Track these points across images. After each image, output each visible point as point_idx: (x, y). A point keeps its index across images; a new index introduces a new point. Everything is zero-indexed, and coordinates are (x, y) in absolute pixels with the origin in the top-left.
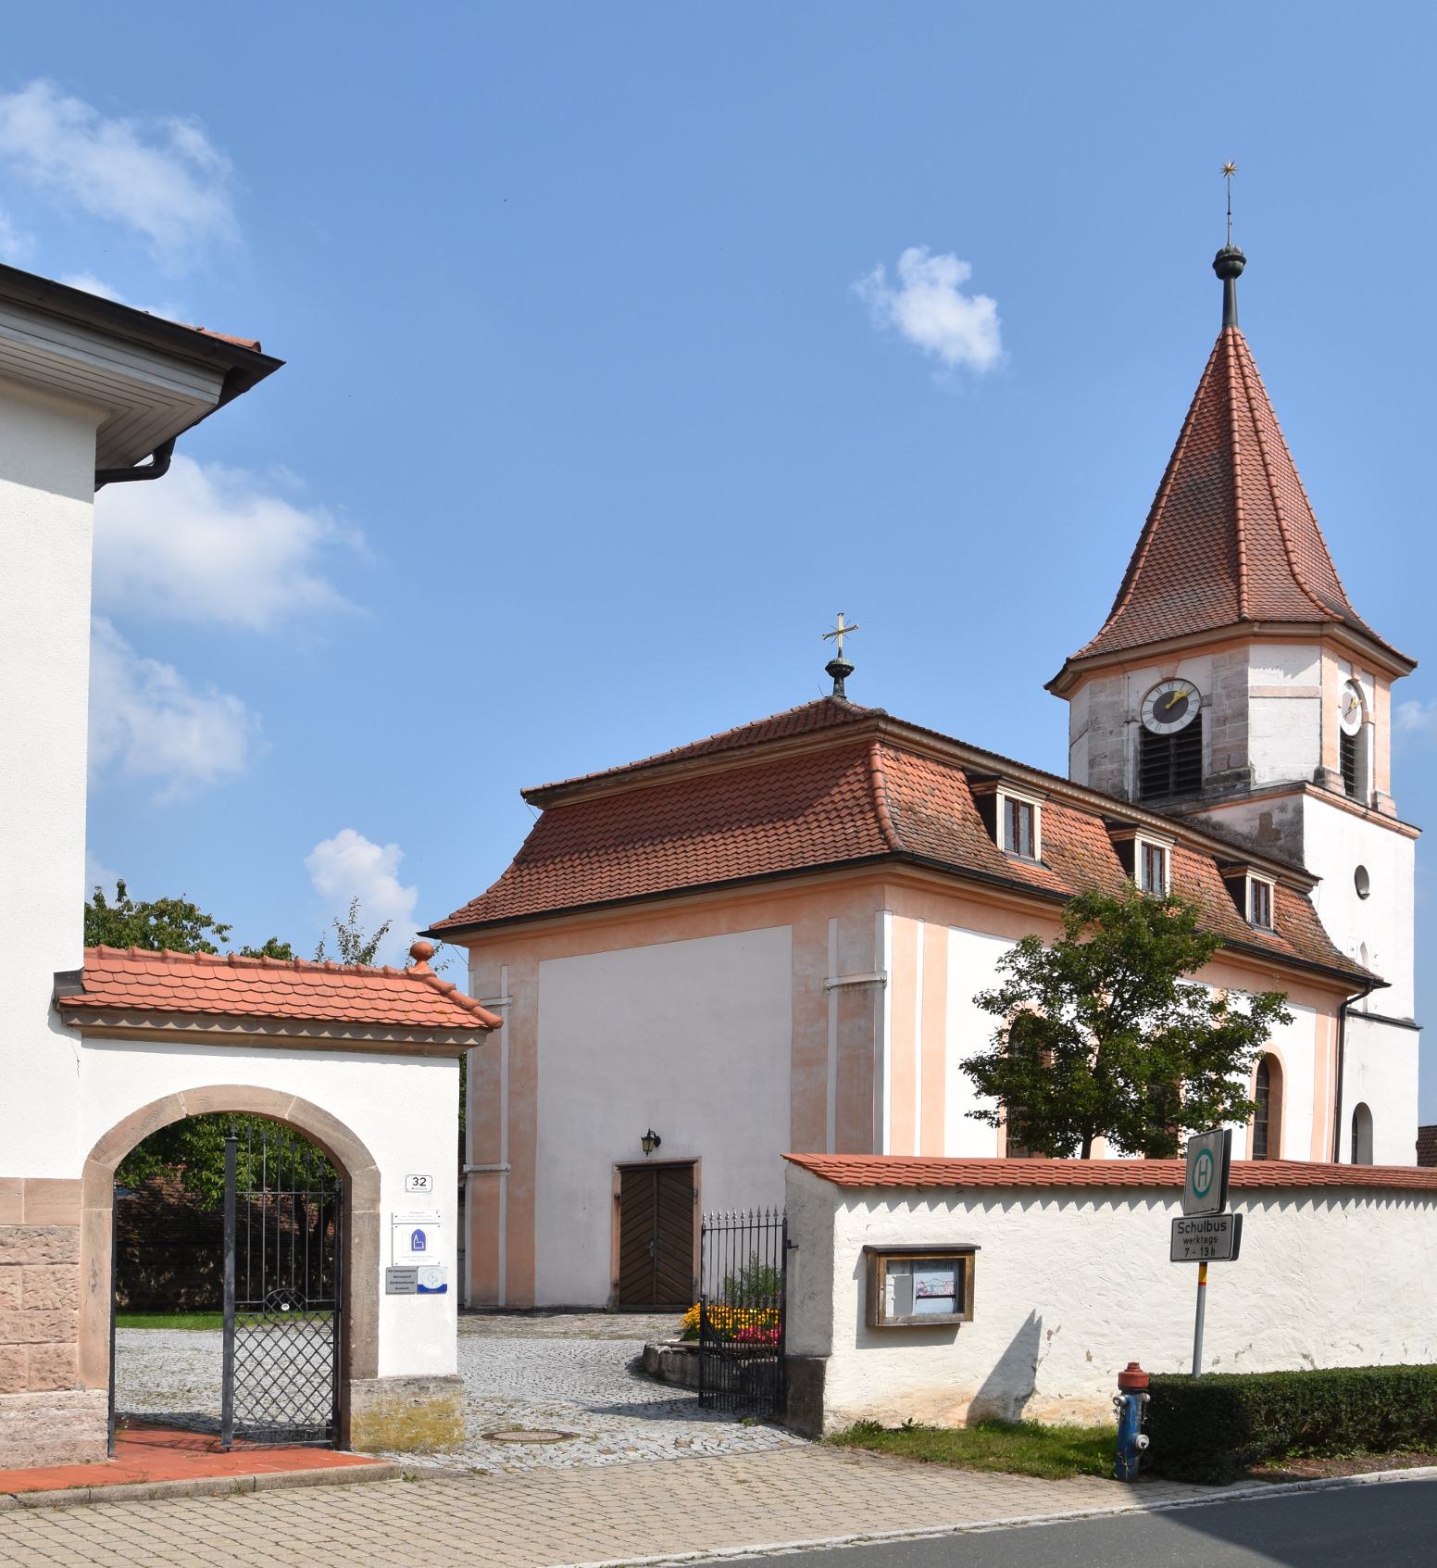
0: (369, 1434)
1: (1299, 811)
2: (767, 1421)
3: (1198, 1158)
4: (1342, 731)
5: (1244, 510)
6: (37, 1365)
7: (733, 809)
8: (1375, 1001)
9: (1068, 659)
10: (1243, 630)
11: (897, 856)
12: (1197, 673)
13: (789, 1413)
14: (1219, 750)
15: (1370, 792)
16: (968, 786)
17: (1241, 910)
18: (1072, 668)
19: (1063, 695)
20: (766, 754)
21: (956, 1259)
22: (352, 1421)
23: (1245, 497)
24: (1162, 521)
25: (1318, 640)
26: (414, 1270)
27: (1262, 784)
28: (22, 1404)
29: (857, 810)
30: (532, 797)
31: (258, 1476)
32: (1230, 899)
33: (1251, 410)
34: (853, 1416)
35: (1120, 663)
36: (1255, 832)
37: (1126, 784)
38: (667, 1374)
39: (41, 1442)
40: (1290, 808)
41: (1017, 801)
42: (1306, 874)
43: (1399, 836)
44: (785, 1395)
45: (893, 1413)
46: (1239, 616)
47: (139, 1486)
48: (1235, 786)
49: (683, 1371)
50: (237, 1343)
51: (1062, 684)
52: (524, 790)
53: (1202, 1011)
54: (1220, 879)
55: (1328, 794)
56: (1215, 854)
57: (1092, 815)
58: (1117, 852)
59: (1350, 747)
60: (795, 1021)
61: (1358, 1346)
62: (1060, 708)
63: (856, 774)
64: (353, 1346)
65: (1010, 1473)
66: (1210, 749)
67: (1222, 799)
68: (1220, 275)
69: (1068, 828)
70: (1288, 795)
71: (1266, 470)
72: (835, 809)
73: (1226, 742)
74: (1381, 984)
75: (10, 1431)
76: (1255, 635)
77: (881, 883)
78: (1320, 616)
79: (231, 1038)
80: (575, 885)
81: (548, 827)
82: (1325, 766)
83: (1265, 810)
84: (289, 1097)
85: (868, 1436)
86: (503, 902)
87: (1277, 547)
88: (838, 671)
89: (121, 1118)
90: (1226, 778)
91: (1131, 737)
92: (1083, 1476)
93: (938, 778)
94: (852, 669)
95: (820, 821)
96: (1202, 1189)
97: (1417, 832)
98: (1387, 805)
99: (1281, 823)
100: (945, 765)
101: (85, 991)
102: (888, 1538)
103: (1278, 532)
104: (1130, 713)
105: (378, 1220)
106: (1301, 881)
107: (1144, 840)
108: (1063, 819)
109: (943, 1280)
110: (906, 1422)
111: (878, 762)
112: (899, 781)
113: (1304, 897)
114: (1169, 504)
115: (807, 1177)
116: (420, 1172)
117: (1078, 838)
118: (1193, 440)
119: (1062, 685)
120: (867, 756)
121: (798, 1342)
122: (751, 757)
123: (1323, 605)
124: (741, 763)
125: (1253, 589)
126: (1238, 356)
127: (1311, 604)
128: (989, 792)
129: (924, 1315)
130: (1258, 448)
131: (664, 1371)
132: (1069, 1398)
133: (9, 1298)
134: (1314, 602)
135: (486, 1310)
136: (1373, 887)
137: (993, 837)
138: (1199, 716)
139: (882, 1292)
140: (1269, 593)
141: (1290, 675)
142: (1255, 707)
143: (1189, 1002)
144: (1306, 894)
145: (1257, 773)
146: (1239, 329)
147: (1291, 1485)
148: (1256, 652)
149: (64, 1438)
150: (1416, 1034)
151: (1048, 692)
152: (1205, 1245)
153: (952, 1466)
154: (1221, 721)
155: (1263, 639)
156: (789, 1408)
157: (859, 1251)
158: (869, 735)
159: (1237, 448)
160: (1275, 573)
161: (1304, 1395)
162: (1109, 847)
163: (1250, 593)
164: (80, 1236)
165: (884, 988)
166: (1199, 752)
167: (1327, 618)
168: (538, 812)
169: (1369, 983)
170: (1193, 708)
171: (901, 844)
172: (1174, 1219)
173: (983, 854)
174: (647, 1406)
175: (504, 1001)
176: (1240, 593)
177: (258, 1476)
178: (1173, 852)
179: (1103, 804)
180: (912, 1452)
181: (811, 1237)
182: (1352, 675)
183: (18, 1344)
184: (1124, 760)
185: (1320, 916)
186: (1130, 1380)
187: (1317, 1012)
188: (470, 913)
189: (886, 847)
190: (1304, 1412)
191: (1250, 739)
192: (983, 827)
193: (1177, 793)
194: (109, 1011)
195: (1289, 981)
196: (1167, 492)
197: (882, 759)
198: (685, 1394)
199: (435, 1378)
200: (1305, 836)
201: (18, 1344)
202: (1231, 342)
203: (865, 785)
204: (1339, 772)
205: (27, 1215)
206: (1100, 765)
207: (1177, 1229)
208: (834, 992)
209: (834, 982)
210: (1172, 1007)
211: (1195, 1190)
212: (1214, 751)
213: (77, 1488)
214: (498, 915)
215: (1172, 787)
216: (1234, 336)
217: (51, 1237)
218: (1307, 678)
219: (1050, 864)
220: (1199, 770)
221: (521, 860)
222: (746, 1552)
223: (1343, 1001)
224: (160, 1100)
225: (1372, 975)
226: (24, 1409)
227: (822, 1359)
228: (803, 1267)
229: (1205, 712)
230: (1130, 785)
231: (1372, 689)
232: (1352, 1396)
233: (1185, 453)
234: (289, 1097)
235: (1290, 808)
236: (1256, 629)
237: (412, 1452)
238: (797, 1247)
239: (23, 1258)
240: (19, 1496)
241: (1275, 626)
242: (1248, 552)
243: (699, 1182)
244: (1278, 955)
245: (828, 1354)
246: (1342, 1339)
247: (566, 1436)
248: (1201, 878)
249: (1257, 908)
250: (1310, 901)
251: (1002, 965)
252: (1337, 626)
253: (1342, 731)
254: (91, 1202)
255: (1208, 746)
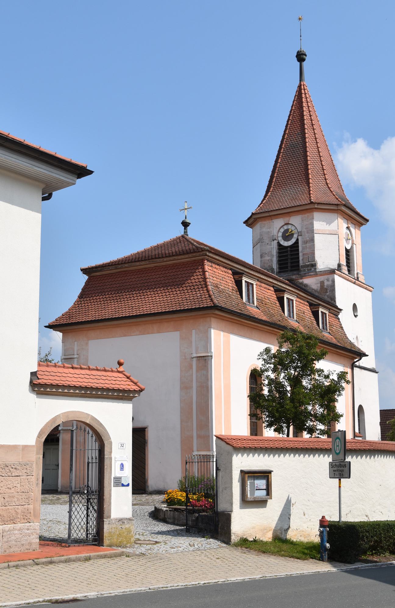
0: (109, 540)
1: (333, 281)
2: (212, 537)
3: (336, 440)
4: (345, 247)
5: (309, 156)
6: (23, 514)
7: (157, 282)
8: (363, 362)
9: (252, 213)
10: (311, 206)
11: (215, 307)
12: (296, 221)
13: (219, 534)
14: (305, 254)
15: (356, 272)
16: (233, 276)
17: (318, 324)
18: (254, 217)
19: (250, 226)
20: (168, 261)
21: (266, 475)
22: (104, 535)
23: (310, 151)
24: (282, 158)
25: (336, 211)
26: (120, 478)
27: (320, 269)
28: (19, 528)
29: (200, 286)
30: (85, 271)
31: (91, 554)
32: (314, 319)
33: (310, 116)
34: (240, 536)
35: (270, 216)
36: (319, 289)
37: (273, 265)
38: (167, 519)
39: (23, 543)
40: (330, 279)
41: (248, 282)
42: (336, 307)
43: (366, 290)
44: (218, 527)
45: (250, 535)
46: (310, 200)
47: (63, 557)
48: (311, 269)
49: (174, 518)
50: (73, 505)
51: (250, 222)
52: (82, 268)
53: (322, 378)
54: (310, 311)
55: (342, 274)
56: (308, 300)
57: (270, 286)
58: (279, 301)
59: (348, 253)
60: (181, 371)
62: (249, 231)
63: (199, 272)
64: (105, 506)
65: (290, 557)
66: (302, 253)
67: (307, 274)
68: (298, 60)
69: (263, 292)
70: (329, 274)
71: (316, 141)
72: (193, 285)
73: (307, 251)
74: (365, 355)
75: (15, 538)
76: (316, 208)
77: (210, 317)
78: (336, 202)
79: (74, 394)
80: (102, 310)
81: (90, 283)
82: (341, 262)
83: (322, 280)
84: (88, 415)
85: (244, 543)
86: (76, 315)
87: (321, 172)
88: (185, 224)
89: (45, 423)
90: (308, 266)
91: (275, 246)
92: (311, 559)
93: (224, 273)
94: (190, 224)
95: (188, 290)
96: (338, 452)
97: (372, 289)
98: (361, 278)
99: (327, 286)
100: (226, 268)
101: (39, 379)
102: (270, 577)
103: (321, 166)
104: (274, 237)
105: (111, 459)
106: (336, 311)
107: (287, 297)
108: (261, 288)
109: (261, 483)
110: (254, 538)
111: (207, 268)
112: (213, 275)
113: (337, 317)
114: (284, 152)
115: (223, 443)
116: (122, 442)
117: (266, 296)
118: (291, 126)
119: (250, 222)
120: (203, 265)
121: (222, 506)
122: (163, 262)
123: (338, 197)
124: (159, 264)
125: (314, 189)
126: (305, 94)
127: (333, 196)
128: (240, 279)
129: (259, 497)
130: (313, 131)
131: (166, 518)
132: (299, 530)
133: (17, 488)
134: (334, 195)
135: (67, 492)
136: (359, 313)
137: (242, 297)
138: (297, 240)
139: (247, 487)
140: (319, 191)
142: (317, 237)
143: (318, 374)
144: (337, 316)
145: (318, 264)
146: (305, 82)
147: (371, 564)
148: (316, 215)
149: (29, 541)
151: (245, 225)
152: (340, 472)
153: (273, 555)
154: (305, 242)
155: (319, 210)
156: (219, 532)
157: (239, 472)
158: (203, 257)
159: (306, 131)
160: (321, 183)
161: (371, 530)
162: (276, 299)
163: (313, 191)
164: (34, 466)
165: (212, 359)
166: (298, 254)
167: (339, 203)
168: (86, 277)
169: (361, 355)
170: (295, 236)
171: (217, 302)
172: (330, 462)
173: (239, 304)
174: (173, 531)
175: (75, 356)
176: (310, 191)
177: (91, 554)
178: (296, 301)
179: (273, 282)
180: (260, 549)
181: (224, 466)
182: (348, 225)
183: (18, 506)
184: (273, 256)
185: (343, 325)
186: (323, 523)
188: (63, 319)
189: (212, 303)
190: (372, 537)
191: (315, 250)
192: (238, 293)
193: (291, 271)
194: (45, 386)
195: (335, 353)
196: (283, 147)
197: (208, 266)
198: (178, 528)
199: (126, 519)
200: (336, 291)
201: (18, 506)
202: (303, 88)
203: (202, 277)
204: (345, 265)
205: (22, 458)
206: (264, 257)
207: (331, 466)
208: (195, 359)
209: (195, 355)
210: (313, 376)
211: (336, 452)
212: (303, 254)
213: (47, 558)
214: (74, 321)
215: (289, 268)
216: (303, 85)
217: (27, 466)
218: (333, 226)
219: (259, 307)
220: (298, 262)
221: (81, 296)
222: (237, 580)
223: (353, 362)
224: (56, 416)
225: (362, 351)
226: (19, 530)
227: (230, 513)
228: (222, 477)
229: (300, 238)
230: (275, 266)
231: (354, 230)
232: (384, 531)
233: (289, 131)
234: (89, 415)
235: (330, 279)
236: (316, 206)
237: (120, 547)
238: (220, 470)
239: (21, 474)
240: (35, 560)
241: (322, 205)
242: (312, 174)
243: (147, 437)
244: (330, 343)
245: (232, 511)
246: (377, 509)
247: (157, 542)
248: (304, 311)
249: (323, 323)
250: (339, 319)
251: (259, 357)
253: (345, 247)
254: (37, 454)
255: (301, 252)
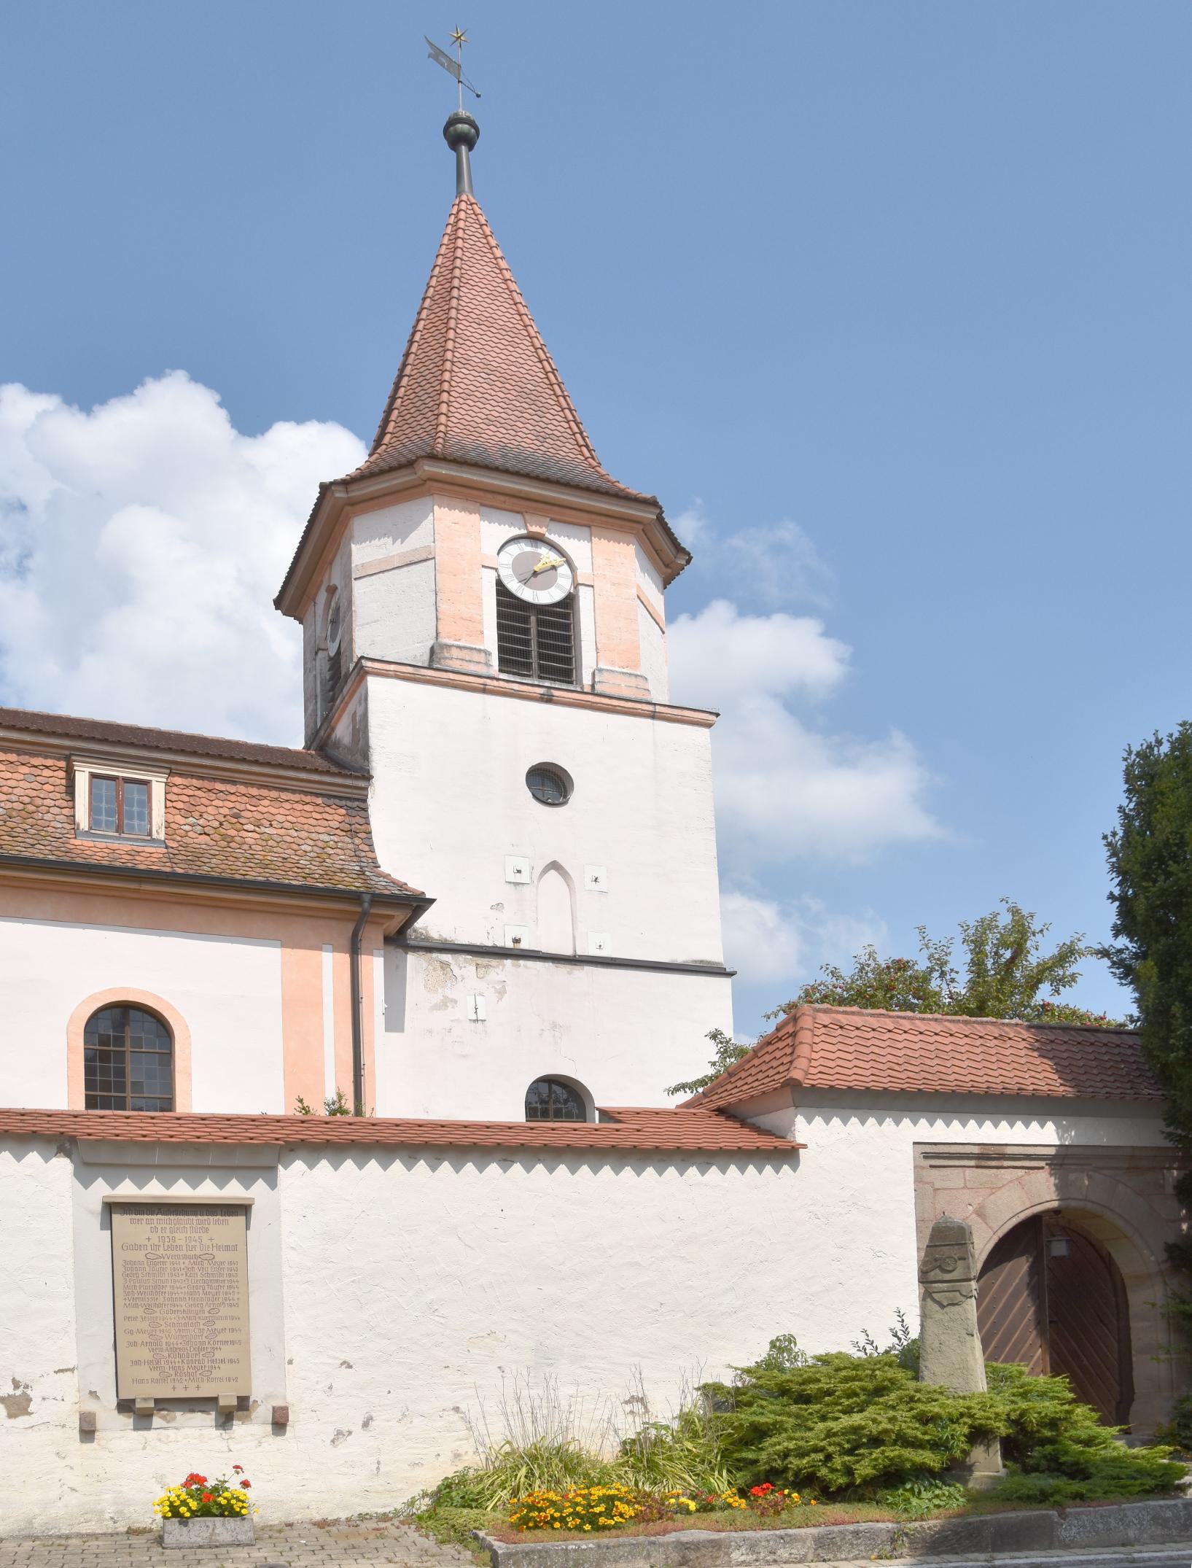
61: (457, 1409)
141: (399, 540)
150: (725, 983)
187: (282, 946)
252: (425, 462)
